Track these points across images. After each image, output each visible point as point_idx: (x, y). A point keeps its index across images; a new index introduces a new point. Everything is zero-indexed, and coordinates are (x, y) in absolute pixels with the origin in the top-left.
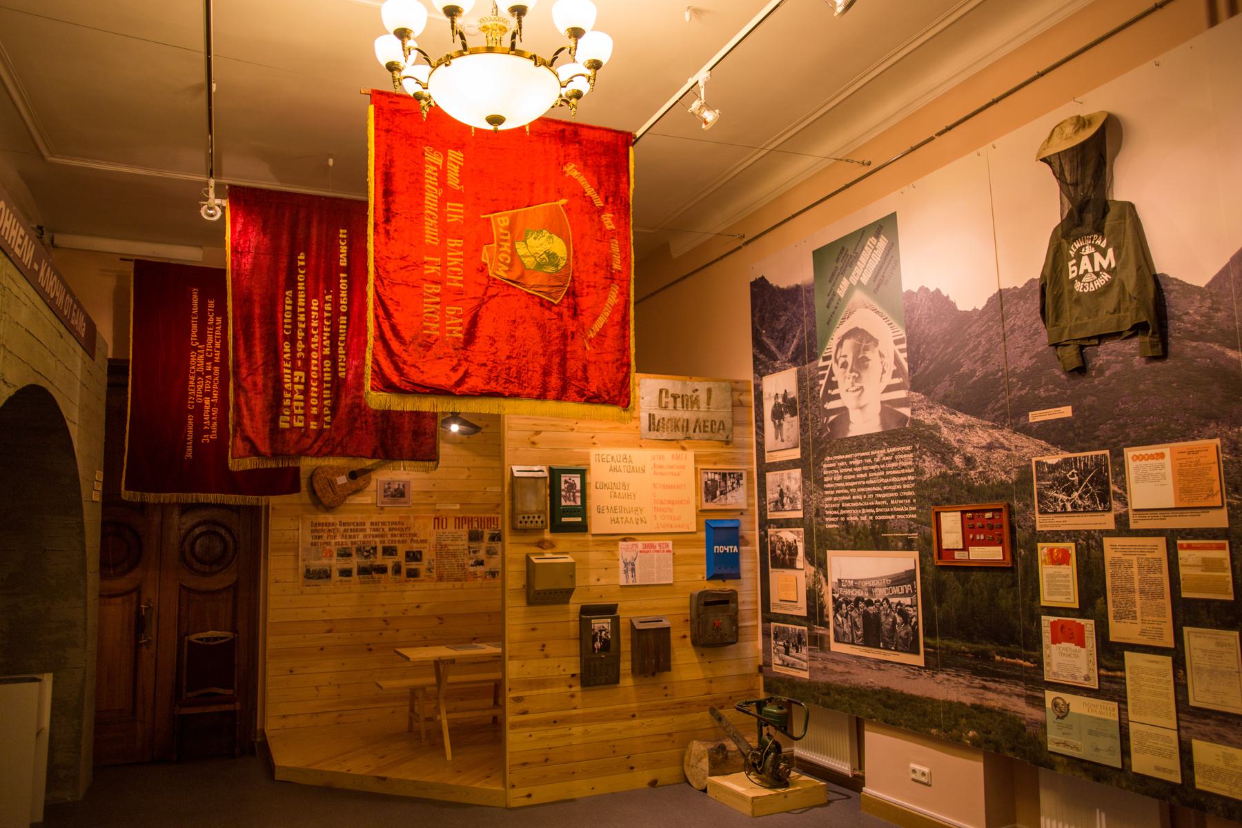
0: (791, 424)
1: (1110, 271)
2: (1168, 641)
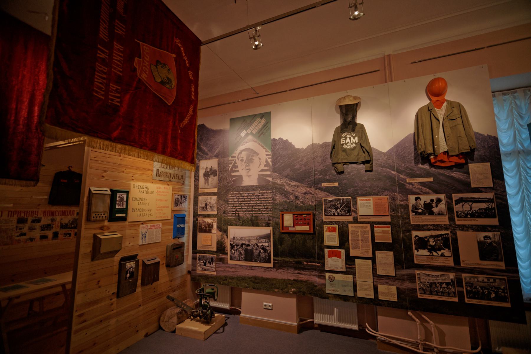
0: (213, 180)
1: (355, 143)
2: (371, 255)
